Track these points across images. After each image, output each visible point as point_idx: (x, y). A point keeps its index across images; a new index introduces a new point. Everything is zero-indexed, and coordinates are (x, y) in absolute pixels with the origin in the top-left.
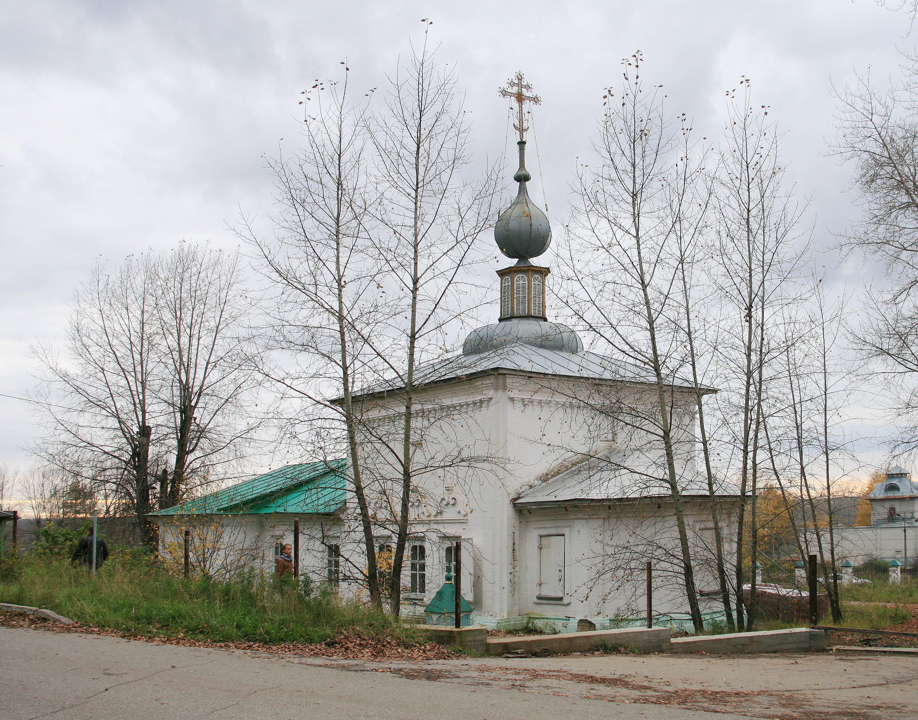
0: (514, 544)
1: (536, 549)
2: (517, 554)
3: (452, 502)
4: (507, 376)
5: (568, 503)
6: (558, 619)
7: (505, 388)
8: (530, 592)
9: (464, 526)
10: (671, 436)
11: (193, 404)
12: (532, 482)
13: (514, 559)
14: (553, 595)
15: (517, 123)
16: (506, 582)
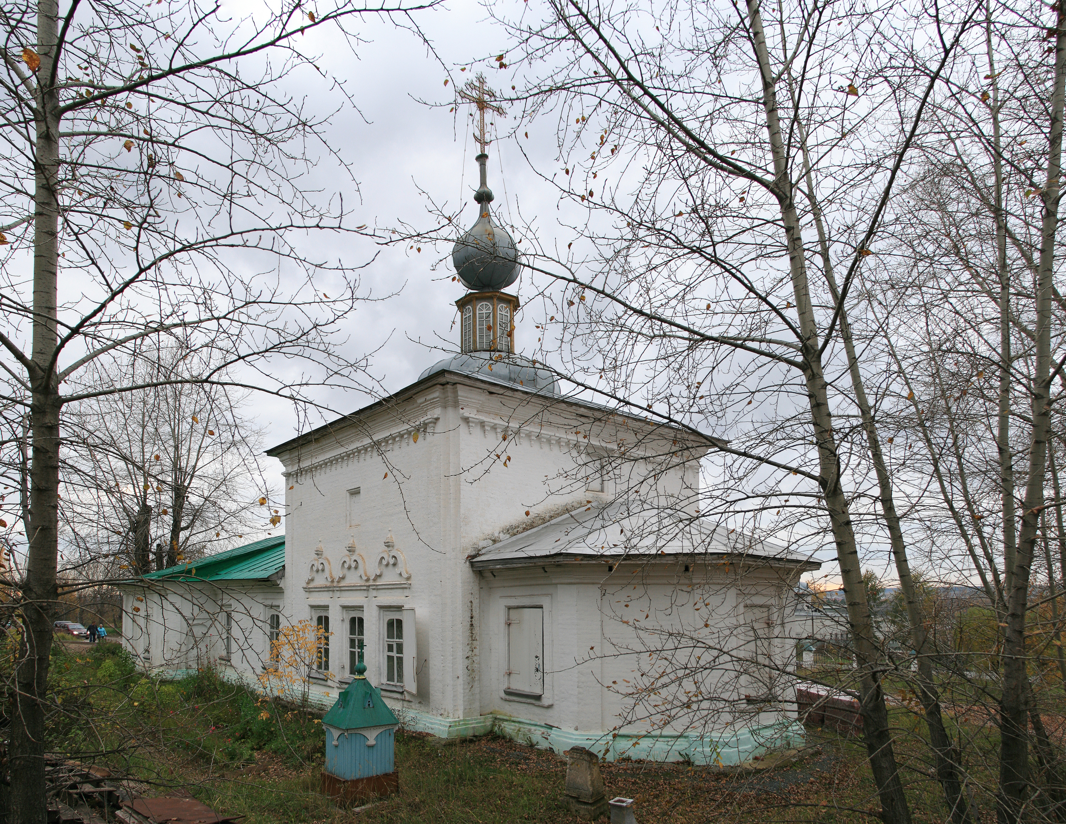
0: (472, 618)
1: (503, 626)
2: (476, 630)
3: (392, 561)
4: (458, 386)
5: (547, 560)
6: (536, 725)
7: (456, 404)
8: (496, 684)
9: (407, 592)
10: (823, 363)
11: (186, 484)
12: (496, 535)
13: (472, 637)
14: (526, 689)
15: (478, 134)
16: (460, 668)
